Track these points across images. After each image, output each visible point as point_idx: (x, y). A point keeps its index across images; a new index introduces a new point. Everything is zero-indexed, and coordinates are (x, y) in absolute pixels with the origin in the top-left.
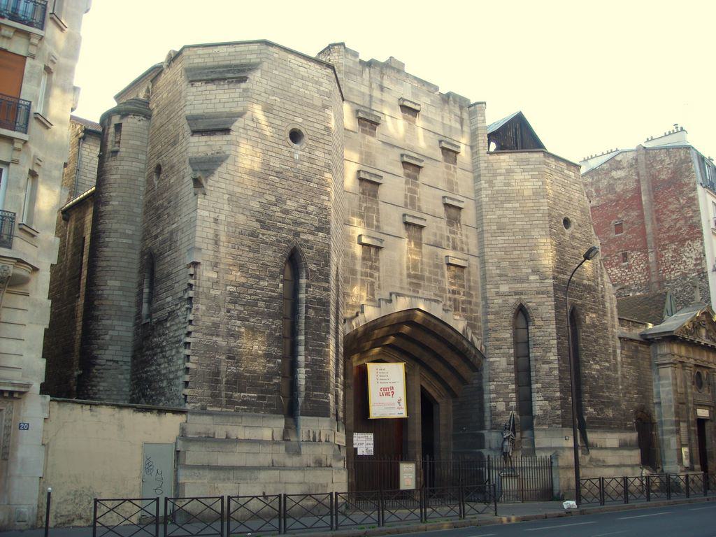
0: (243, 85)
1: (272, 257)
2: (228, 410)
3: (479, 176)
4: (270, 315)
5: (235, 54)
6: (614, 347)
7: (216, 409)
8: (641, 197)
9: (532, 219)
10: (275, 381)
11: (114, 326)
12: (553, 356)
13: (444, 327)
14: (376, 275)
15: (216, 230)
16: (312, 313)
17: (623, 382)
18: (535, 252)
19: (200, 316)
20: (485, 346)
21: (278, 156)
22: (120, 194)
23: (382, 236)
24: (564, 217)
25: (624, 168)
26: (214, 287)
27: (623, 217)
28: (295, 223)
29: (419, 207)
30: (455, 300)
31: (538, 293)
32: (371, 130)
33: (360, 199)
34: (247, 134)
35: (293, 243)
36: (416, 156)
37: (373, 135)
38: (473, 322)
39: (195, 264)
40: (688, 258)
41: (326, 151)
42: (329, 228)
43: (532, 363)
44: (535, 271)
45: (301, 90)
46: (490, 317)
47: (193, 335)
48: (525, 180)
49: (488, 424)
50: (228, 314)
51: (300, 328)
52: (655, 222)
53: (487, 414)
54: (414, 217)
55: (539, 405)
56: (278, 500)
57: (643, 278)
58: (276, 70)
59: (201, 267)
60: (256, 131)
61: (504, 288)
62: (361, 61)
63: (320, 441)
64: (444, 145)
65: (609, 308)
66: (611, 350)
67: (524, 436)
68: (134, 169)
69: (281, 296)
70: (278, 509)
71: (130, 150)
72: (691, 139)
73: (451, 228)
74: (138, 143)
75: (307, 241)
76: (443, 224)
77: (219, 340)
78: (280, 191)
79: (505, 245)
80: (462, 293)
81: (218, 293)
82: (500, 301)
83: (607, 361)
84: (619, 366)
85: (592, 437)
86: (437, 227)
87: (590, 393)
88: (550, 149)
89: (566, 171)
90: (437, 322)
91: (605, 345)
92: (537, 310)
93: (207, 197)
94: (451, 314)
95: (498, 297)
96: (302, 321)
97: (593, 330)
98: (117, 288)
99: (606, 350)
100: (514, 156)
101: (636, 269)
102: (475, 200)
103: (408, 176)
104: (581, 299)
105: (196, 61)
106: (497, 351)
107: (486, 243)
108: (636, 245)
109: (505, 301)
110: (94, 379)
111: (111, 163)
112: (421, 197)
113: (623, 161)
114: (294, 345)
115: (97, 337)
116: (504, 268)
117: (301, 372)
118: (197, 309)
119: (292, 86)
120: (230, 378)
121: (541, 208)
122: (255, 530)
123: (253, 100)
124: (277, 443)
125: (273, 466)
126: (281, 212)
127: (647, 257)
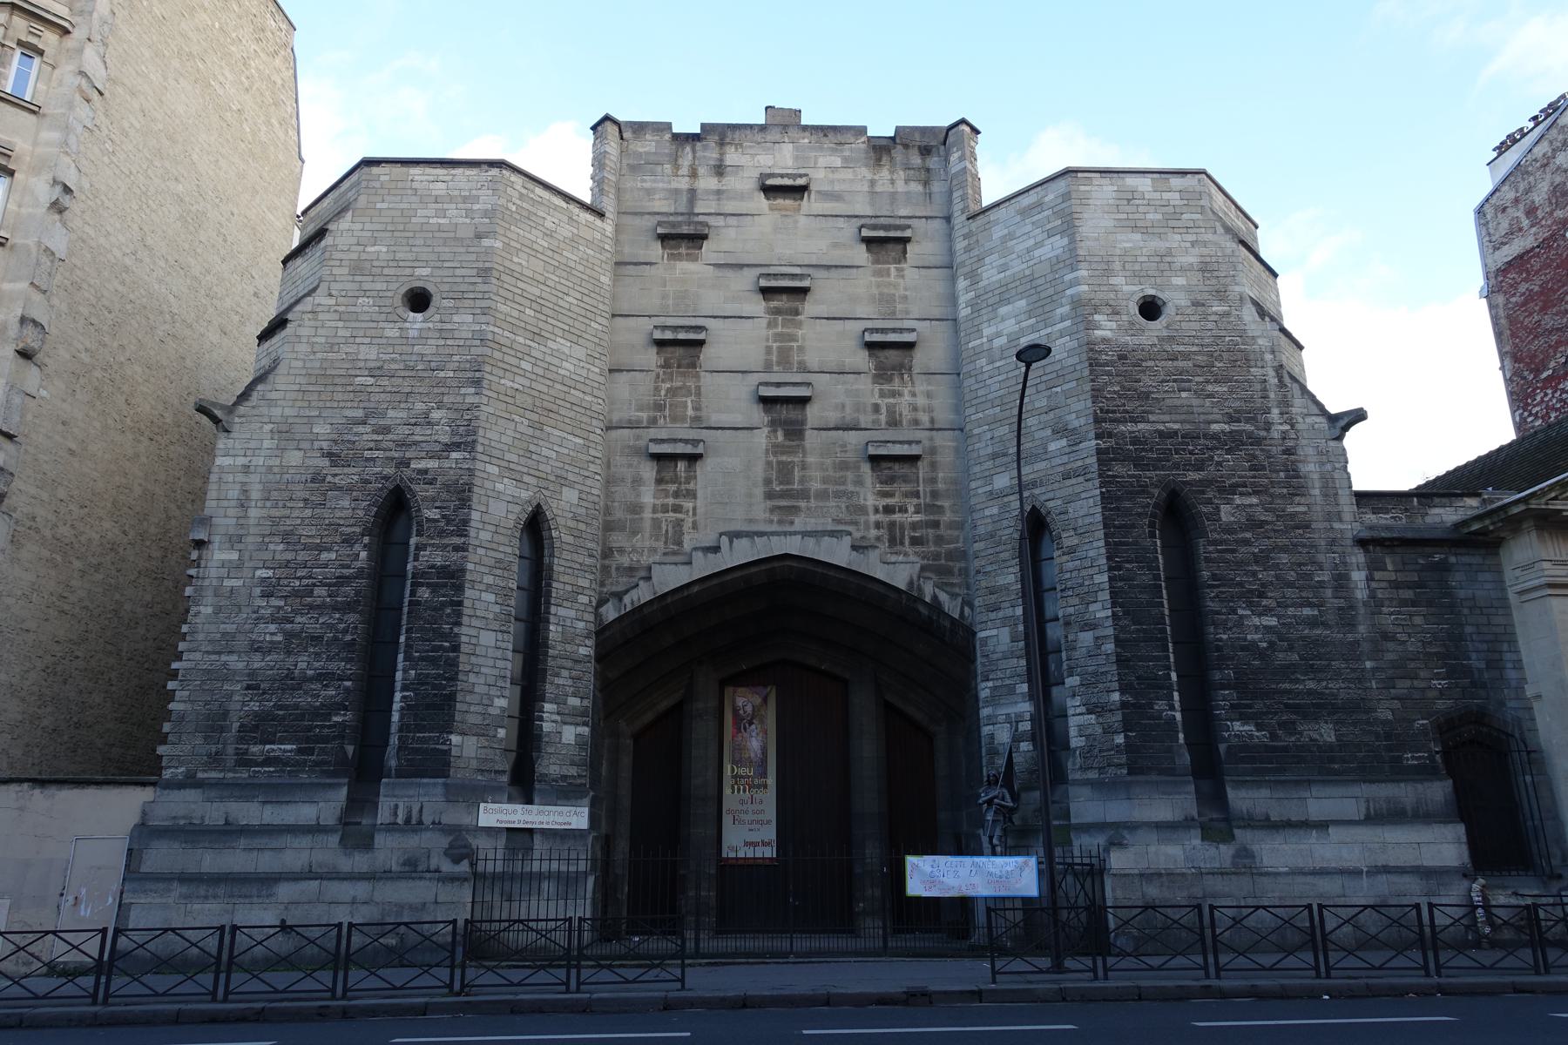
1: (350, 511)
2: (237, 775)
4: (335, 608)
7: (214, 775)
12: (1101, 611)
16: (424, 593)
18: (1059, 389)
23: (704, 434)
30: (892, 525)
36: (797, 271)
37: (695, 259)
38: (943, 562)
39: (200, 544)
50: (254, 616)
54: (778, 385)
55: (1079, 724)
56: (1306, 912)
63: (420, 822)
65: (1316, 476)
69: (360, 573)
73: (886, 387)
75: (426, 471)
80: (911, 509)
82: (995, 511)
83: (1310, 605)
92: (1066, 513)
93: (232, 435)
95: (991, 503)
97: (1248, 535)
104: (1200, 469)
106: (993, 615)
109: (1004, 508)
120: (245, 721)
125: (309, 875)
126: (375, 432)
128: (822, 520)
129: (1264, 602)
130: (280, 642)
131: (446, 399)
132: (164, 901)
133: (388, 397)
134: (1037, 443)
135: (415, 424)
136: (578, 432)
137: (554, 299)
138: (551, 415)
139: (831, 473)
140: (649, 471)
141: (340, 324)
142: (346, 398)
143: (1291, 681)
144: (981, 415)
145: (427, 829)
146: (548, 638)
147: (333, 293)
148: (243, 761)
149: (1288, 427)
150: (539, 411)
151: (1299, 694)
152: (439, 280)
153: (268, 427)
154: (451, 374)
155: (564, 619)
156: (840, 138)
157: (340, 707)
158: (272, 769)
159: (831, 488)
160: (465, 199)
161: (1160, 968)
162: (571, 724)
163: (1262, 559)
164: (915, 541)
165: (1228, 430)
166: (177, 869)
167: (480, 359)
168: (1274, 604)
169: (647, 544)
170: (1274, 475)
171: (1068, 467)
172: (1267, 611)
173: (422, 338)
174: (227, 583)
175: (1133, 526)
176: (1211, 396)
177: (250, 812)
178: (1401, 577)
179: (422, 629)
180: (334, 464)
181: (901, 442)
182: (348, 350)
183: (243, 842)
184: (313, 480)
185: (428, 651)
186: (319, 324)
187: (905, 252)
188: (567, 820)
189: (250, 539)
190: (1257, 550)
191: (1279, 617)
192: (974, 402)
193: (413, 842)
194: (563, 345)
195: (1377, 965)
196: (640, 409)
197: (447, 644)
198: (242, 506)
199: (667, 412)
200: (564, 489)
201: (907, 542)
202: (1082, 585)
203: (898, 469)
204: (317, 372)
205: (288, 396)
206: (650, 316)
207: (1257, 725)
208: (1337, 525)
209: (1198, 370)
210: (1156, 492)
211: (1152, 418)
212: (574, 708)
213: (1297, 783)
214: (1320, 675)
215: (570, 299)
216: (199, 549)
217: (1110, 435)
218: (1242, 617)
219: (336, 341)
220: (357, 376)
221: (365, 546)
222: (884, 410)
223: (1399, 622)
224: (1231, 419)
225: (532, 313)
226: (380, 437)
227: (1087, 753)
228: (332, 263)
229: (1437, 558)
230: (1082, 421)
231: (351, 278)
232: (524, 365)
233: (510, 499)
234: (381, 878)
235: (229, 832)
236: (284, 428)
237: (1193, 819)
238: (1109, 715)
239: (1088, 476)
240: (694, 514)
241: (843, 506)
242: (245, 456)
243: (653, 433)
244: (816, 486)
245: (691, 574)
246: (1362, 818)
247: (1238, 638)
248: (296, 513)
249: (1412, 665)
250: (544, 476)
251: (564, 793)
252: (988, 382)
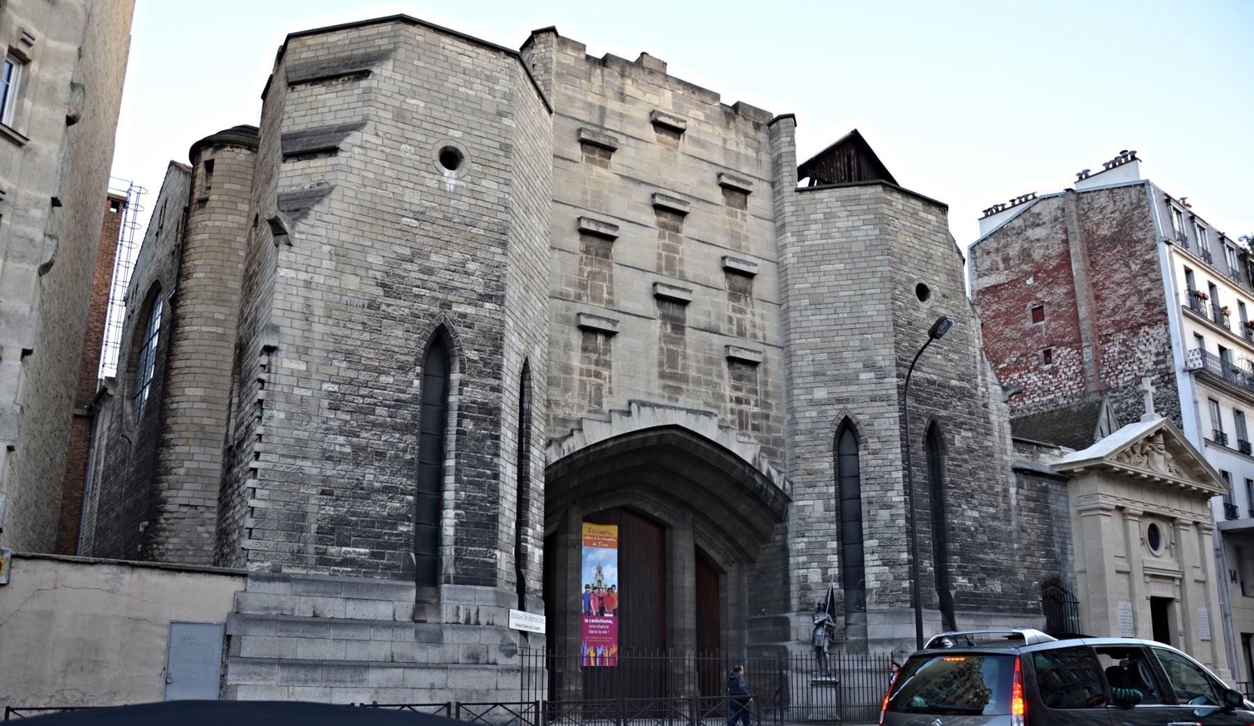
0: (364, 83)
3: (783, 226)
4: (395, 428)
5: (359, 40)
6: (1006, 483)
7: (297, 571)
8: (1070, 264)
9: (863, 286)
10: (402, 529)
11: (193, 454)
12: (897, 496)
13: (722, 454)
14: (606, 373)
15: (307, 299)
16: (469, 425)
18: (869, 336)
19: (275, 429)
20: (791, 483)
21: (417, 187)
22: (208, 262)
23: (616, 316)
24: (917, 283)
25: (1044, 223)
26: (300, 384)
27: (1045, 296)
28: (444, 287)
29: (682, 272)
30: (741, 412)
31: (873, 399)
32: (602, 159)
33: (581, 259)
34: (365, 155)
35: (439, 319)
37: (606, 166)
38: (771, 446)
39: (269, 350)
40: (1144, 353)
41: (502, 181)
42: (503, 296)
43: (864, 508)
44: (870, 366)
45: (461, 89)
46: (797, 438)
47: (262, 457)
48: (855, 228)
49: (794, 602)
50: (324, 426)
51: (449, 448)
52: (1093, 302)
53: (794, 588)
54: (671, 287)
55: (874, 573)
57: (1075, 387)
58: (419, 59)
59: (281, 354)
60: (382, 151)
61: (821, 394)
62: (588, 58)
63: (478, 623)
64: (724, 180)
65: (996, 424)
66: (999, 489)
67: (851, 621)
68: (231, 225)
71: (226, 198)
72: (1145, 171)
73: (736, 304)
74: (238, 187)
75: (464, 316)
76: (723, 299)
77: (308, 463)
78: (420, 240)
79: (822, 328)
80: (752, 403)
81: (308, 393)
82: (814, 414)
83: (992, 506)
84: (1014, 512)
86: (712, 302)
87: (961, 554)
88: (903, 184)
89: (922, 214)
90: (709, 447)
91: (989, 480)
92: (872, 425)
93: (293, 249)
94: (733, 434)
95: (811, 408)
96: (452, 437)
97: (967, 457)
98: (198, 399)
99: (991, 488)
100: (837, 193)
101: (1065, 374)
102: (778, 263)
103: (664, 226)
104: (946, 409)
105: (304, 55)
106: (810, 490)
107: (792, 325)
108: (1063, 337)
110: (161, 533)
111: (197, 218)
112: (685, 258)
113: (1043, 213)
114: (440, 473)
115: (168, 471)
116: (821, 363)
117: (449, 516)
118: (271, 418)
119: (446, 84)
120: (323, 523)
121: (879, 269)
123: (377, 105)
124: (403, 626)
125: (391, 663)
127: (1080, 354)
130: (349, 454)
131: (478, 254)
132: (267, 683)
133: (431, 242)
134: (851, 371)
135: (454, 271)
140: (576, 339)
141: (387, 164)
142: (394, 235)
144: (804, 341)
145: (484, 628)
147: (380, 133)
148: (324, 561)
152: (469, 145)
153: (326, 248)
154: (482, 232)
157: (404, 518)
158: (349, 569)
159: (703, 377)
160: (488, 78)
163: (972, 473)
164: (755, 428)
166: (275, 654)
167: (505, 224)
169: (576, 401)
171: (875, 393)
173: (456, 193)
174: (297, 391)
176: (951, 361)
177: (336, 608)
179: (468, 457)
180: (387, 295)
181: (750, 351)
182: (396, 191)
183: (332, 633)
184: (369, 307)
185: (473, 476)
186: (368, 159)
187: (746, 202)
189: (315, 353)
191: (980, 512)
192: (798, 330)
193: (475, 639)
197: (489, 472)
198: (307, 320)
199: (589, 292)
201: (750, 427)
202: (882, 477)
204: (368, 205)
205: (343, 221)
206: (575, 207)
207: (969, 579)
208: (1005, 457)
213: (986, 616)
216: (268, 355)
218: (964, 510)
219: (384, 179)
220: (403, 216)
221: (418, 375)
222: (735, 322)
224: (961, 379)
226: (426, 277)
227: (882, 592)
228: (377, 105)
229: (1044, 484)
230: (887, 363)
231: (394, 123)
234: (451, 669)
235: (317, 622)
236: (342, 252)
238: (899, 567)
239: (890, 402)
240: (610, 382)
241: (710, 392)
242: (307, 272)
243: (579, 308)
245: (611, 432)
248: (356, 335)
252: (811, 318)
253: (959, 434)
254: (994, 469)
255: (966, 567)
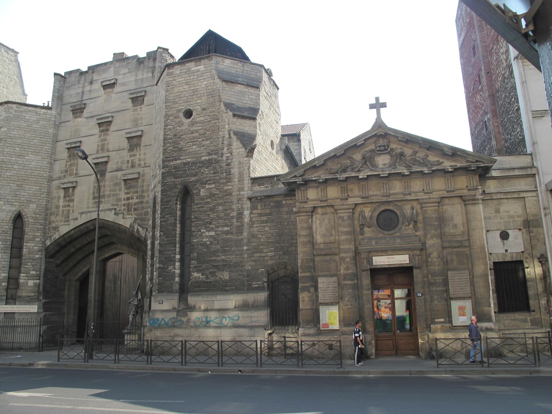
14: (72, 204)
17: (249, 242)
29: (107, 149)
37: (80, 117)
56: (181, 343)
65: (237, 173)
70: (217, 350)
73: (132, 153)
80: (135, 198)
83: (227, 226)
85: (192, 300)
87: (198, 259)
97: (209, 200)
99: (228, 215)
122: (239, 362)
128: (108, 205)
129: (211, 226)
136: (36, 185)
137: (28, 142)
138: (25, 181)
139: (112, 188)
143: (216, 256)
146: (22, 253)
149: (229, 155)
150: (21, 180)
151: (218, 261)
155: (29, 247)
156: (129, 61)
161: (323, 364)
162: (32, 280)
163: (212, 210)
164: (135, 210)
165: (208, 159)
168: (214, 226)
169: (60, 219)
170: (222, 175)
172: (212, 230)
175: (170, 201)
176: (204, 146)
178: (263, 212)
187: (143, 100)
188: (30, 309)
190: (211, 206)
191: (215, 231)
194: (32, 157)
195: (239, 362)
196: (61, 173)
200: (30, 204)
203: (132, 183)
209: (200, 136)
210: (179, 187)
211: (182, 158)
212: (33, 274)
214: (227, 253)
215: (35, 141)
217: (167, 167)
218: (202, 232)
222: (130, 162)
223: (259, 230)
224: (209, 154)
225: (19, 149)
232: (15, 167)
233: (8, 211)
237: (175, 309)
244: (107, 193)
246: (233, 307)
247: (200, 241)
249: (261, 247)
250: (22, 201)
251: (29, 301)
253: (204, 188)
254: (231, 202)
255: (200, 267)
